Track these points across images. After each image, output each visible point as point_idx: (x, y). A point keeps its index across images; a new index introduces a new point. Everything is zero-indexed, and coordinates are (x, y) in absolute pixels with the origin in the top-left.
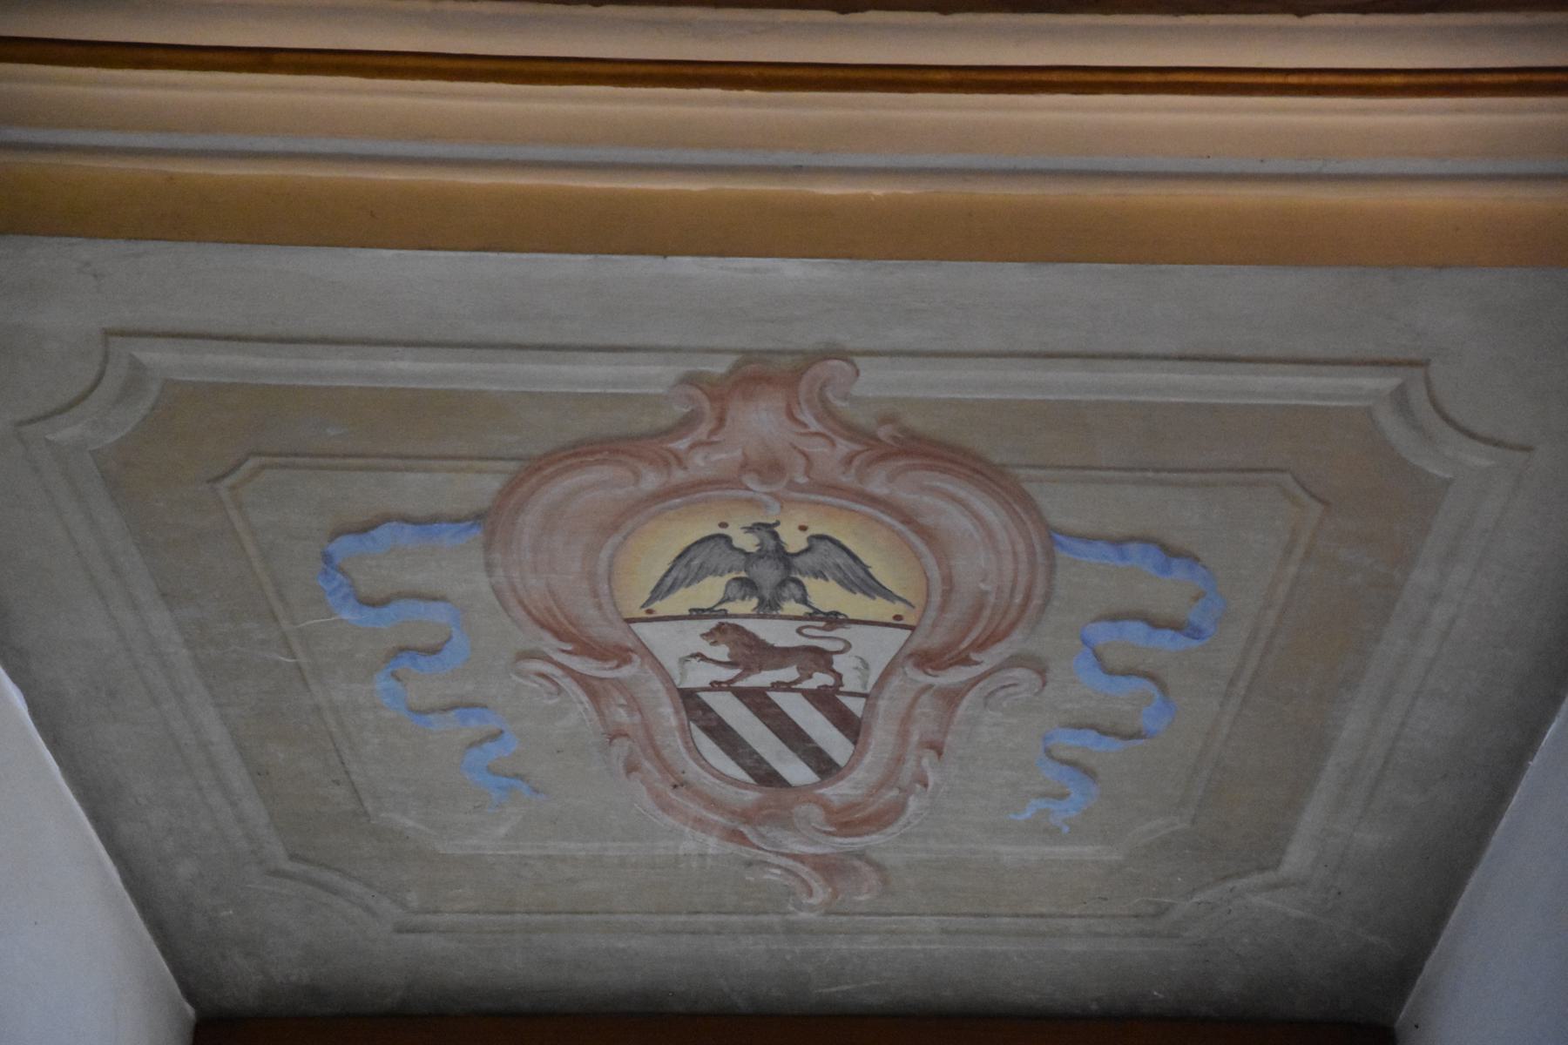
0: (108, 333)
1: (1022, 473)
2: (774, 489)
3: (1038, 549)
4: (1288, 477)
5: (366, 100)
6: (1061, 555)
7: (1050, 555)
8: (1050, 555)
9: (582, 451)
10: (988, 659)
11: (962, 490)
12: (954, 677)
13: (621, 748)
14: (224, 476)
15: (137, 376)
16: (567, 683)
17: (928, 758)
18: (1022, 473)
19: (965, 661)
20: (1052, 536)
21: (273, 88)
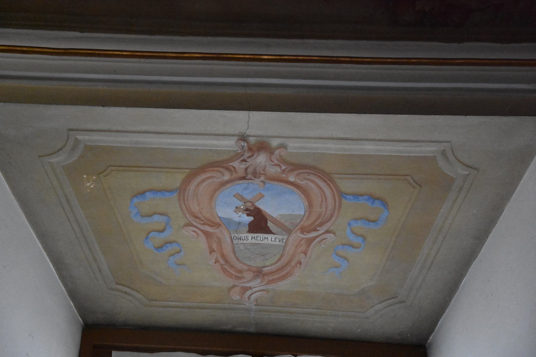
0: (69, 130)
1: (334, 176)
2: (261, 180)
3: (315, 173)
4: (409, 178)
5: (126, 64)
6: (344, 201)
7: (340, 201)
8: (340, 201)
9: (203, 169)
10: (322, 230)
11: (312, 177)
12: (313, 234)
13: (215, 255)
14: (102, 173)
15: (77, 142)
16: (199, 232)
17: (303, 255)
18: (334, 176)
19: (315, 230)
20: (342, 195)
21: (32, 58)
